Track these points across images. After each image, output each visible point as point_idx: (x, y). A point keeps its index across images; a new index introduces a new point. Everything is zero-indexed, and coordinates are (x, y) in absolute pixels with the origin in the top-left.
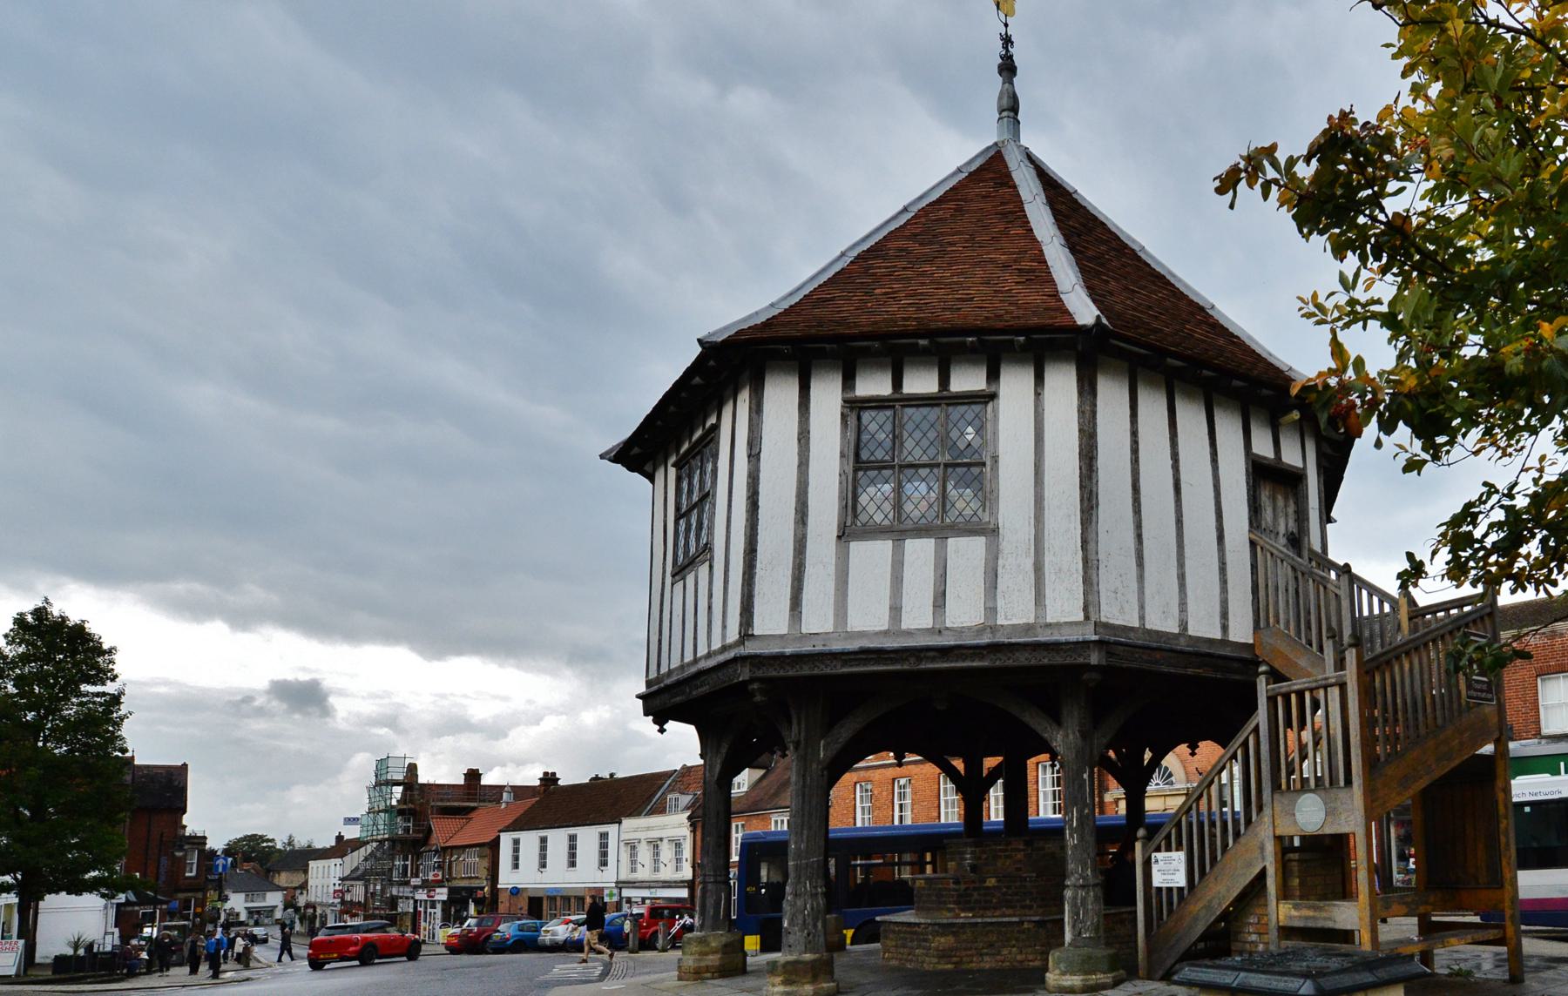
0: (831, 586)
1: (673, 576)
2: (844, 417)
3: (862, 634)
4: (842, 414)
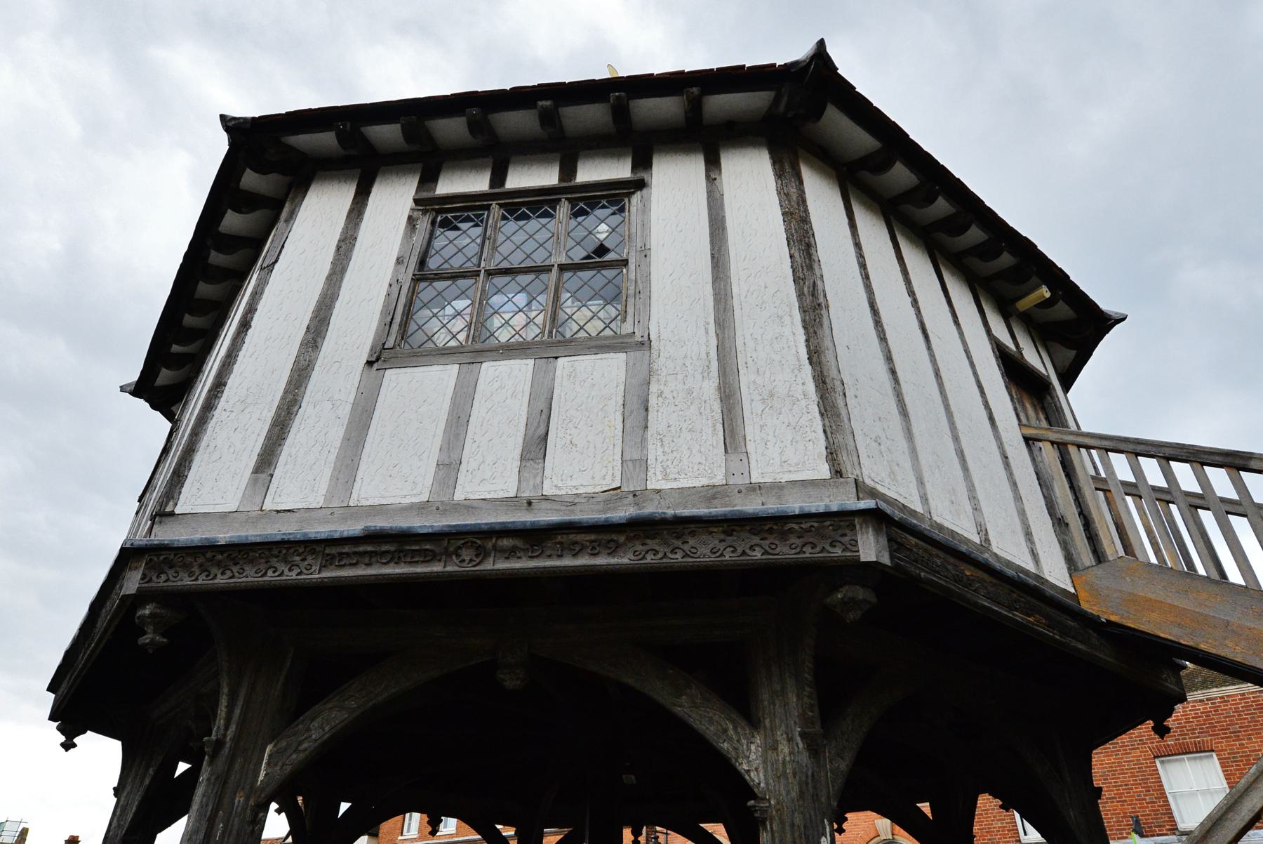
0: (337, 434)
4: (410, 218)
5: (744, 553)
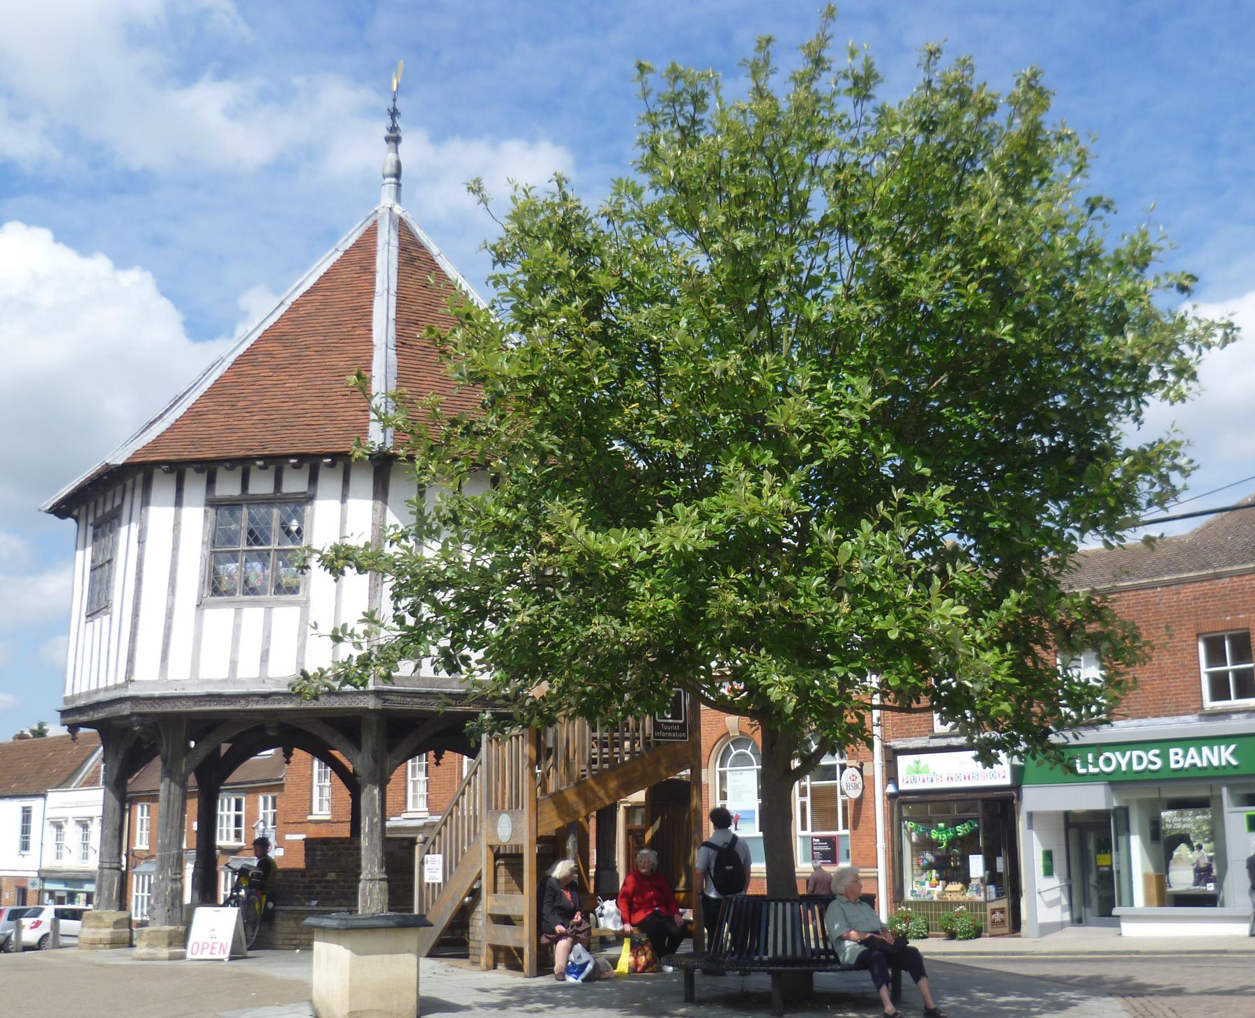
1: (87, 617)
3: (209, 682)
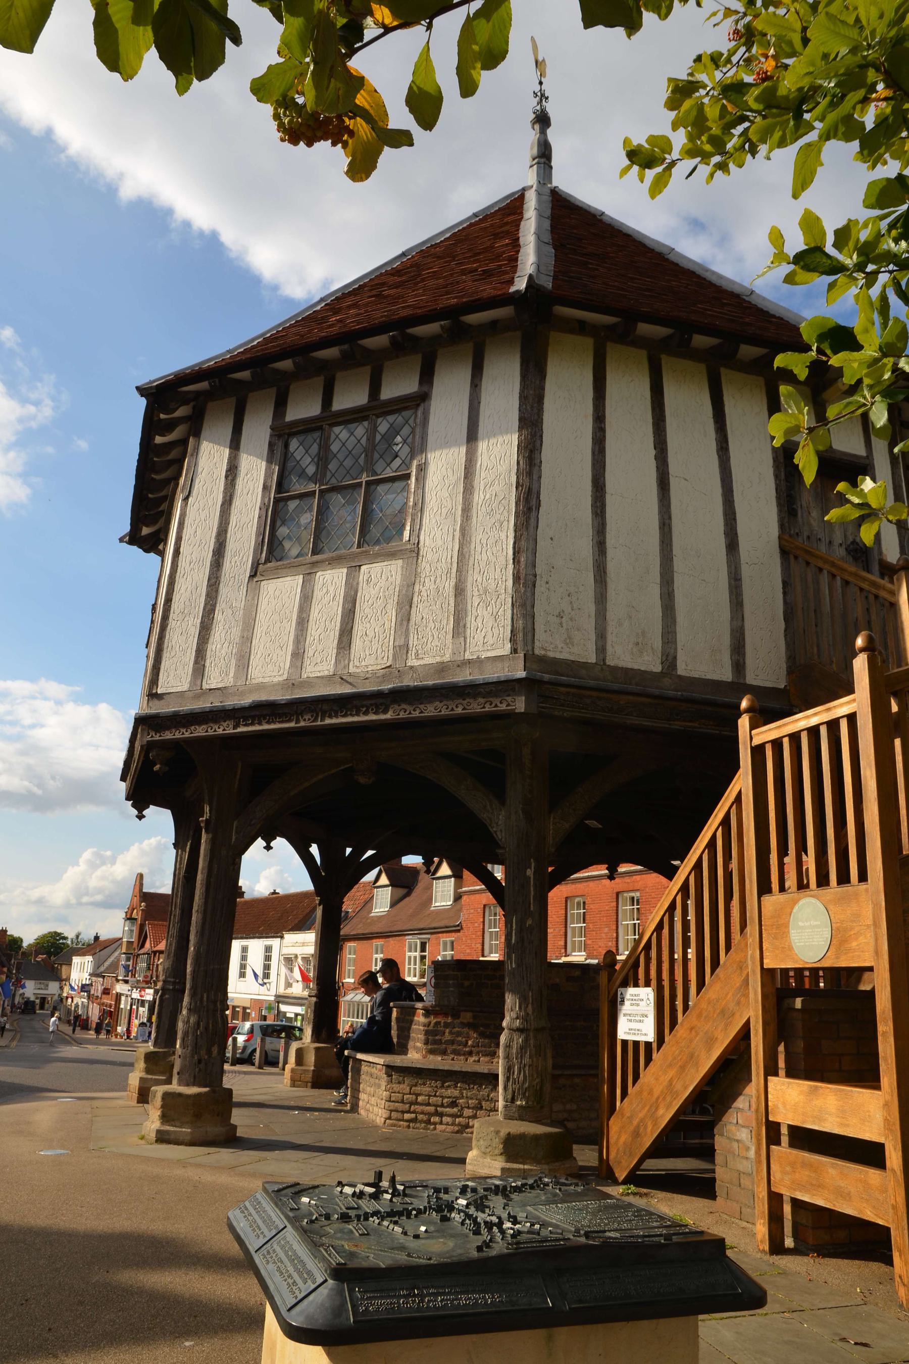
2: (271, 445)
5: (452, 710)
